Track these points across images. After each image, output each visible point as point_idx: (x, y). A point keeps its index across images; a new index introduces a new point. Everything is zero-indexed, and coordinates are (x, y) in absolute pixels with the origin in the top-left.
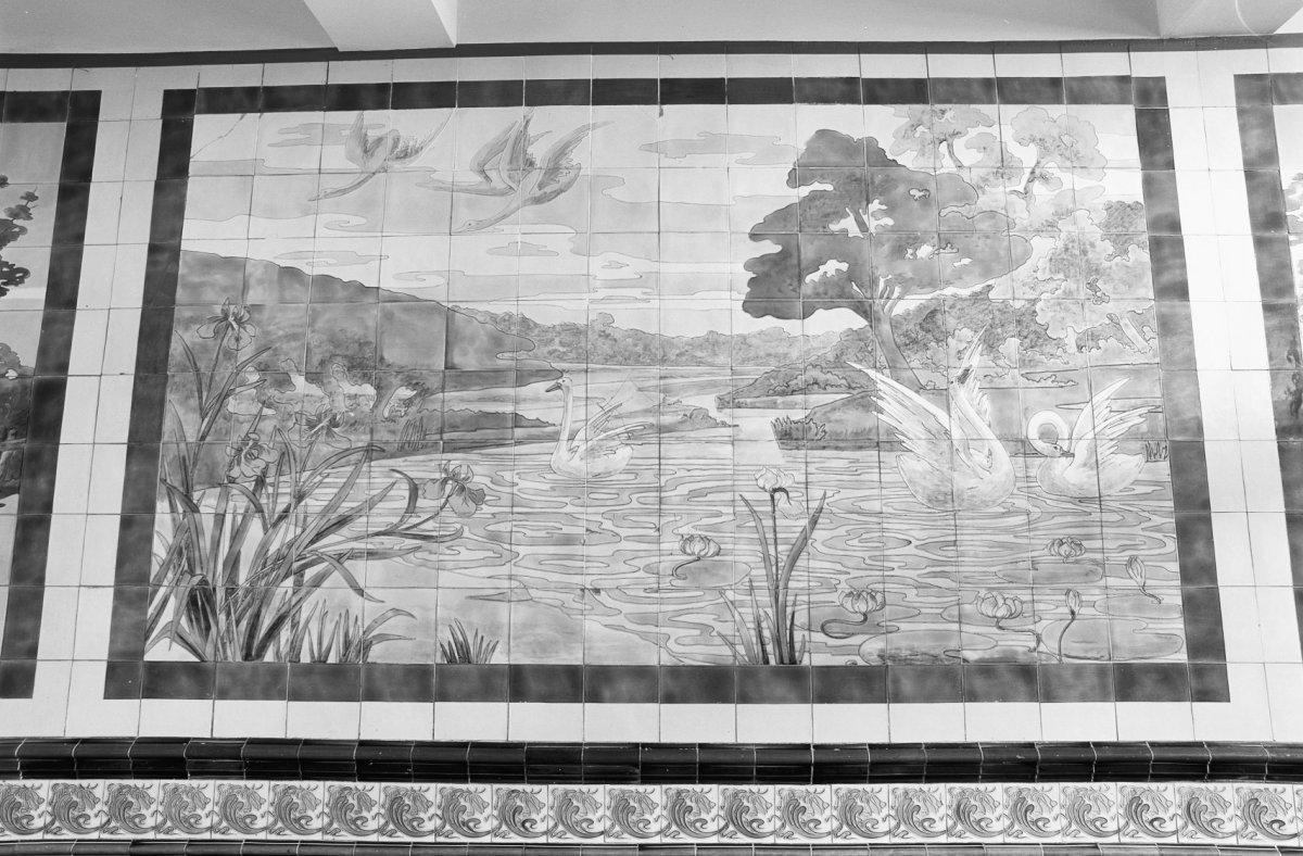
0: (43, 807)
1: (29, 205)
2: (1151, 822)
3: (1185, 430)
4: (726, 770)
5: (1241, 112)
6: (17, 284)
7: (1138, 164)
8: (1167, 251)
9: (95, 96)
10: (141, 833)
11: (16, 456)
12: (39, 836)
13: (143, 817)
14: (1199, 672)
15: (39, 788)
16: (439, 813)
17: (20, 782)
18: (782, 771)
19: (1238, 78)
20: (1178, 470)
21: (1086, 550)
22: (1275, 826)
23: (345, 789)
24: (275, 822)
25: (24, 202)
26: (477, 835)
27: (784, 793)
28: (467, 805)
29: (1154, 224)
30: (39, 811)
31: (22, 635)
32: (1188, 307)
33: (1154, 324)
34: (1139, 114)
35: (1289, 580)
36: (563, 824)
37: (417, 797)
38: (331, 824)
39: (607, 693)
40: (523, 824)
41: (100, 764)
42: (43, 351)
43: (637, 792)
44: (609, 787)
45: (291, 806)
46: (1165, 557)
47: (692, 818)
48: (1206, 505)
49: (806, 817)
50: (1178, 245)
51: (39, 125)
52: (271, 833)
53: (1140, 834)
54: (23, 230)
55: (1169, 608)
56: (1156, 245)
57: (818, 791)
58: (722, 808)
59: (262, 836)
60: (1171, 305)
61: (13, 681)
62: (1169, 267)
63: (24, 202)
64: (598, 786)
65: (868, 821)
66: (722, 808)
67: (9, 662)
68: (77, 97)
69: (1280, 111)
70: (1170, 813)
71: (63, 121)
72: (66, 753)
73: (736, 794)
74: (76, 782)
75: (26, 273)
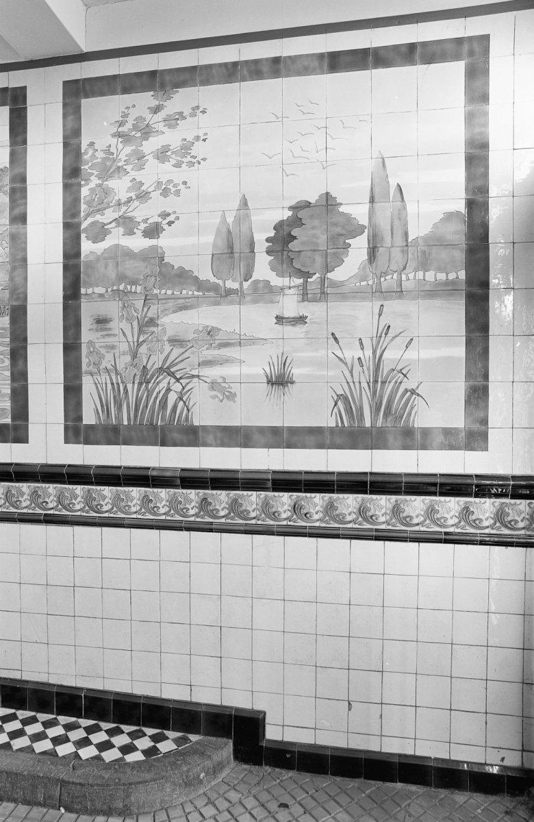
2: (124, 507)
3: (18, 299)
4: (82, 478)
5: (65, 105)
7: (8, 143)
8: (18, 195)
9: (23, 89)
13: (218, 511)
14: (16, 428)
15: (347, 499)
16: (168, 504)
19: (65, 83)
20: (13, 321)
22: (44, 504)
23: (503, 503)
26: (445, 526)
27: (141, 492)
28: (510, 512)
29: (13, 180)
30: (106, 502)
32: (26, 228)
33: (8, 239)
34: (12, 111)
35: (62, 380)
36: (264, 513)
40: (306, 515)
41: (82, 478)
43: (69, 489)
46: (4, 369)
48: (25, 340)
49: (337, 512)
50: (24, 191)
53: (147, 514)
55: (4, 395)
56: (13, 192)
60: (17, 228)
61: (16, 432)
62: (18, 205)
64: (521, 501)
69: (85, 103)
70: (106, 502)
72: (8, 470)
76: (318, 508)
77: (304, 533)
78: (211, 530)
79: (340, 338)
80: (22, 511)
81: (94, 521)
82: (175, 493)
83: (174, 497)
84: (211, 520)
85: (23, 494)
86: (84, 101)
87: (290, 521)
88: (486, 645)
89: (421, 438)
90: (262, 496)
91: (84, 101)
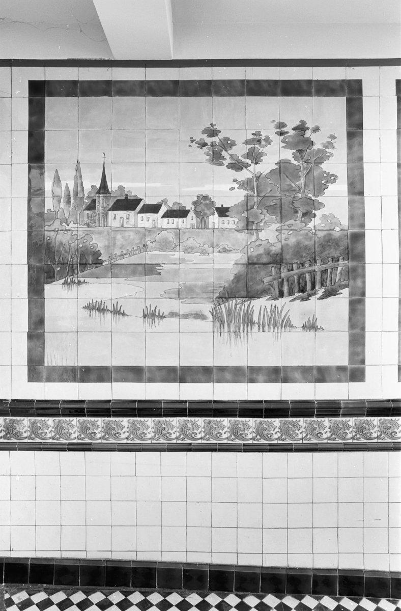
0: (376, 429)
1: (333, 141)
6: (332, 183)
9: (359, 82)
10: (71, 440)
11: (345, 269)
12: (375, 441)
13: (95, 434)
17: (365, 418)
18: (97, 412)
21: (147, 313)
24: (231, 436)
25: (330, 140)
30: (375, 430)
31: (357, 354)
36: (34, 434)
37: (44, 424)
38: (282, 436)
39: (188, 378)
42: (351, 217)
43: (268, 421)
44: (229, 419)
45: (62, 428)
47: (390, 431)
51: (331, 98)
52: (229, 440)
54: (331, 154)
57: (397, 419)
58: (204, 428)
59: (276, 442)
63: (330, 140)
65: (19, 432)
66: (204, 428)
67: (352, 366)
68: (349, 83)
69: (49, 101)
71: (344, 96)
73: (210, 422)
74: (390, 418)
75: (336, 177)
76: (26, 428)
77: (316, 449)
78: (190, 450)
79: (347, 298)
80: (298, 442)
81: (215, 447)
82: (134, 421)
83: (134, 424)
84: (190, 442)
85: (223, 427)
86: (47, 99)
87: (153, 440)
88: (213, 526)
89: (80, 374)
90: (7, 421)
91: (47, 99)
